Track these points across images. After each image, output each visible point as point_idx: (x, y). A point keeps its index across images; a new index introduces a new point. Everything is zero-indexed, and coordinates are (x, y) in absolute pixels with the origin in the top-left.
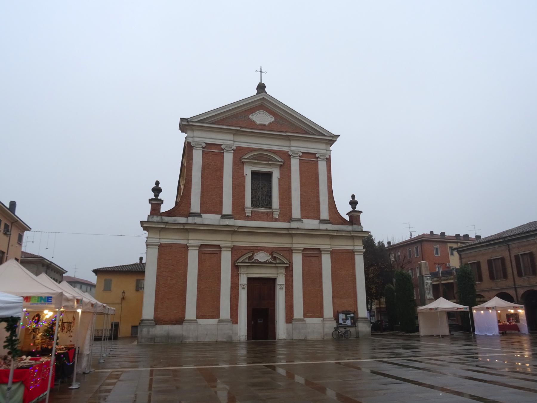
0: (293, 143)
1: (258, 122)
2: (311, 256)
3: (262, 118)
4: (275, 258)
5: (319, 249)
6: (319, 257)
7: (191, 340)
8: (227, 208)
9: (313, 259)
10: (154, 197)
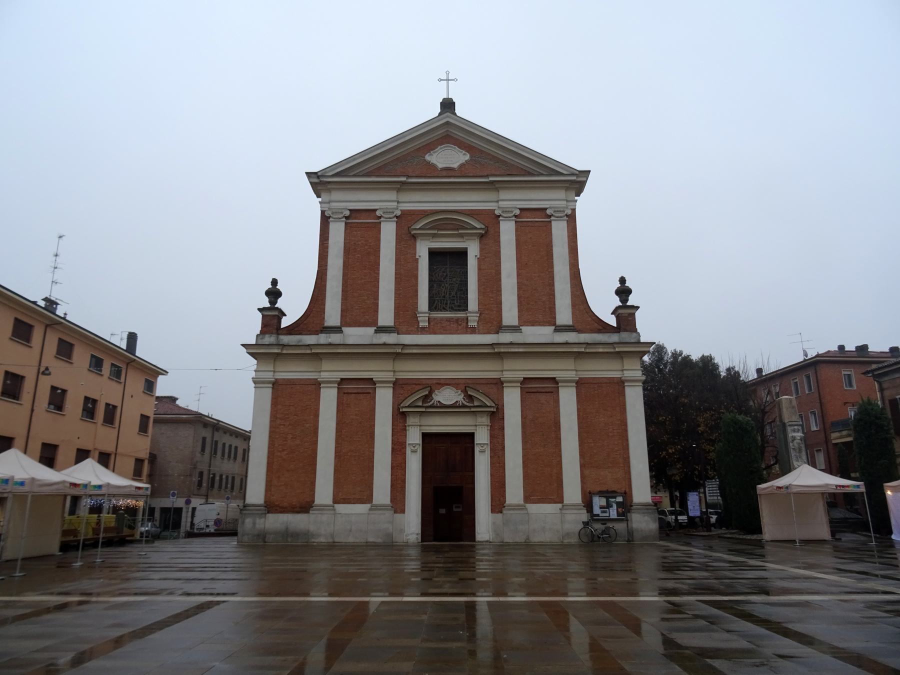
0: (504, 195)
1: (440, 166)
2: (538, 392)
3: (448, 158)
5: (554, 378)
6: (555, 393)
7: (322, 540)
9: (543, 398)
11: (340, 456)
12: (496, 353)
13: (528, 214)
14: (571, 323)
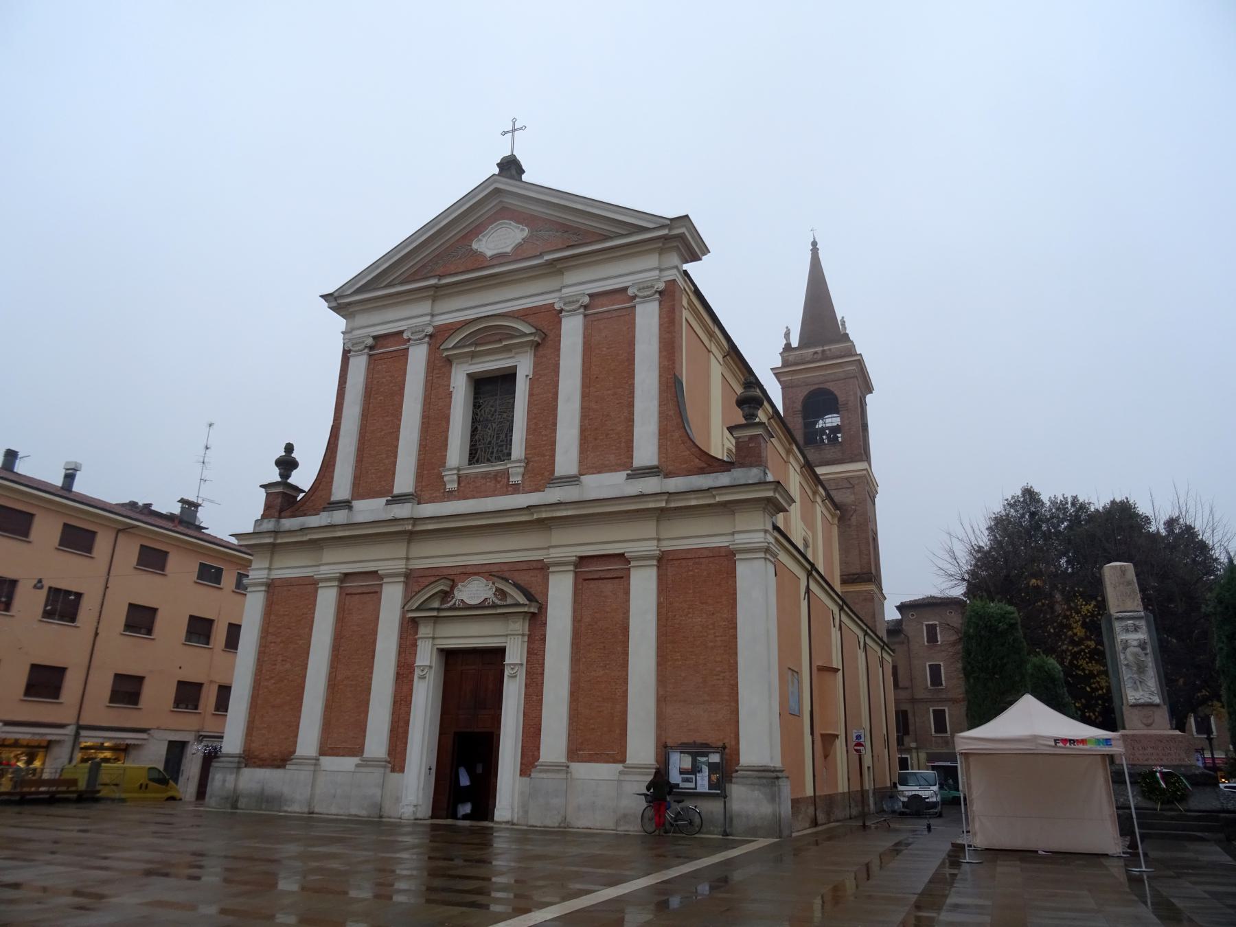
0: (571, 277)
1: (489, 253)
2: (601, 576)
3: (499, 240)
5: (623, 554)
6: (623, 578)
7: (296, 808)
8: (404, 480)
9: (608, 587)
10: (743, 421)
12: (541, 522)
14: (655, 462)
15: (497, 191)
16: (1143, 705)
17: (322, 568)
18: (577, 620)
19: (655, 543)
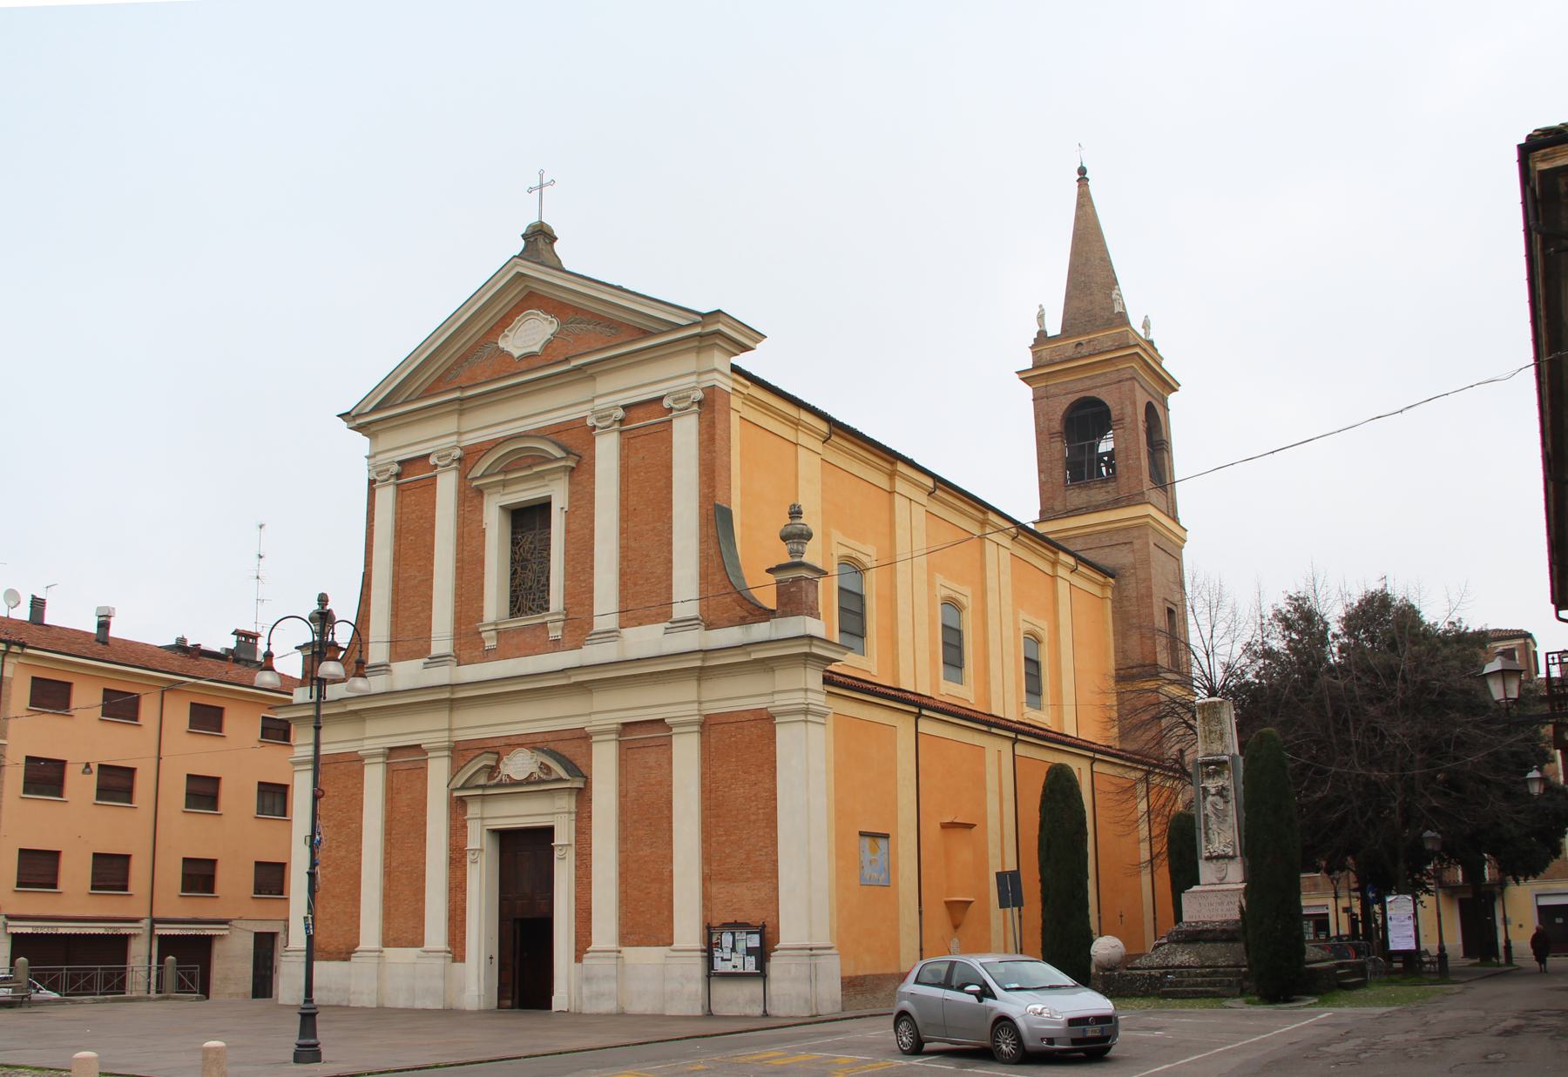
0: (604, 384)
1: (517, 353)
3: (530, 335)
4: (548, 769)
11: (389, 873)
13: (640, 412)
15: (520, 275)
16: (1218, 857)
17: (366, 742)
18: (623, 795)
19: (695, 706)
